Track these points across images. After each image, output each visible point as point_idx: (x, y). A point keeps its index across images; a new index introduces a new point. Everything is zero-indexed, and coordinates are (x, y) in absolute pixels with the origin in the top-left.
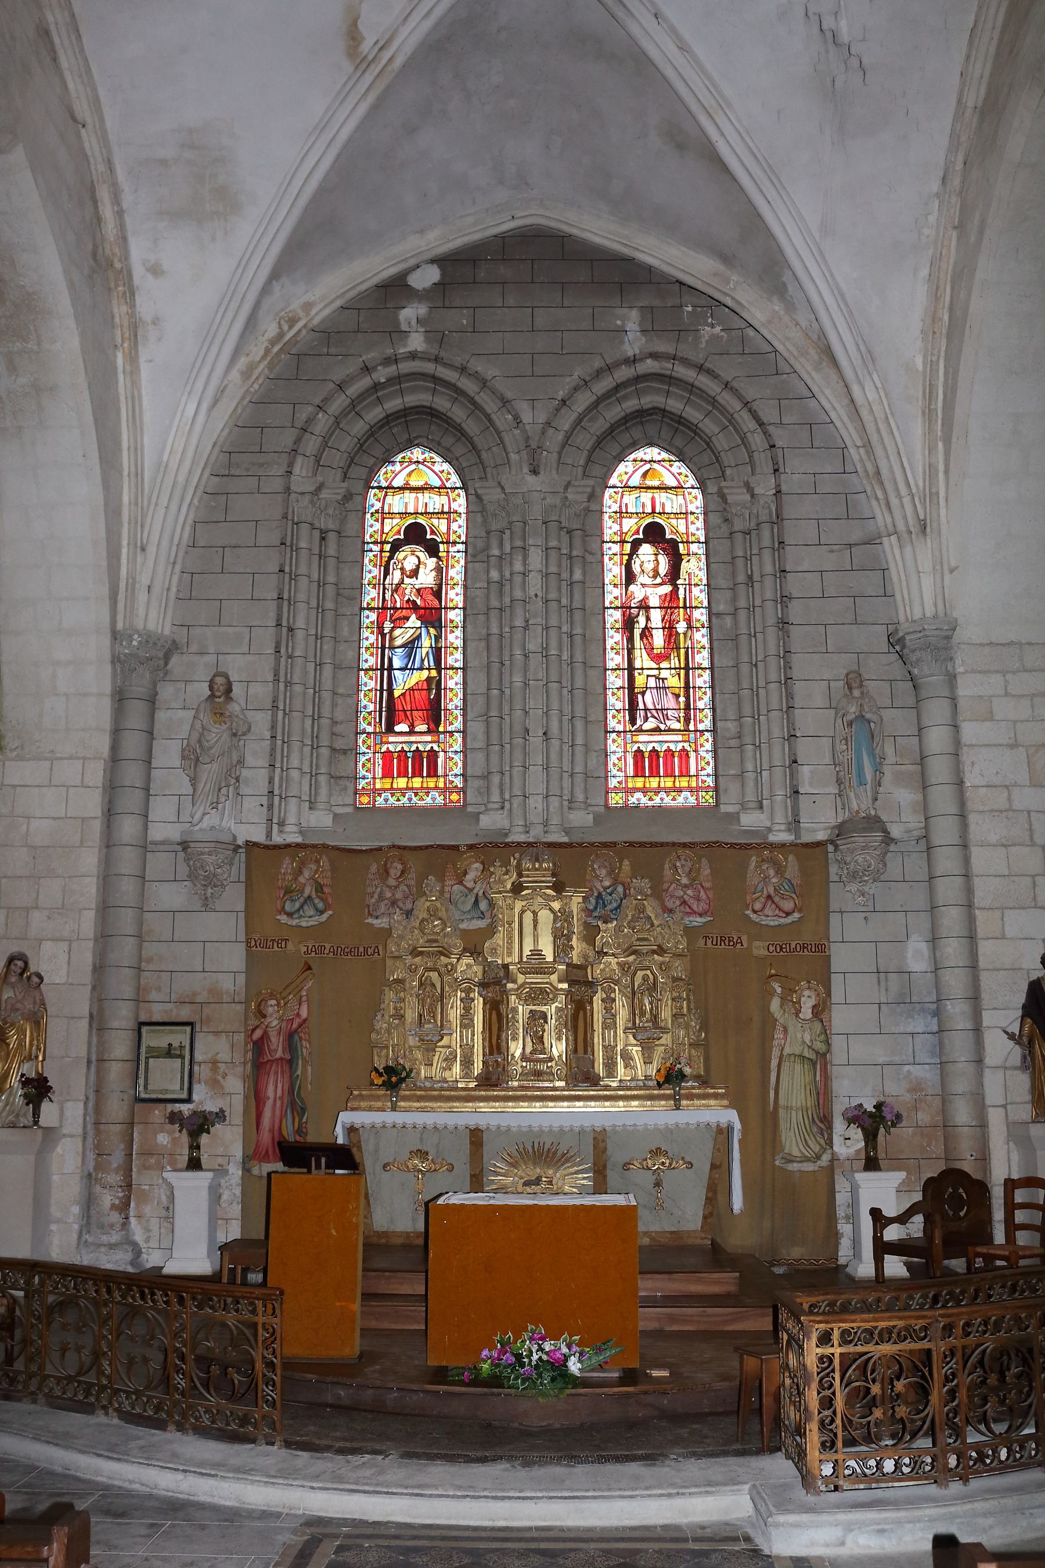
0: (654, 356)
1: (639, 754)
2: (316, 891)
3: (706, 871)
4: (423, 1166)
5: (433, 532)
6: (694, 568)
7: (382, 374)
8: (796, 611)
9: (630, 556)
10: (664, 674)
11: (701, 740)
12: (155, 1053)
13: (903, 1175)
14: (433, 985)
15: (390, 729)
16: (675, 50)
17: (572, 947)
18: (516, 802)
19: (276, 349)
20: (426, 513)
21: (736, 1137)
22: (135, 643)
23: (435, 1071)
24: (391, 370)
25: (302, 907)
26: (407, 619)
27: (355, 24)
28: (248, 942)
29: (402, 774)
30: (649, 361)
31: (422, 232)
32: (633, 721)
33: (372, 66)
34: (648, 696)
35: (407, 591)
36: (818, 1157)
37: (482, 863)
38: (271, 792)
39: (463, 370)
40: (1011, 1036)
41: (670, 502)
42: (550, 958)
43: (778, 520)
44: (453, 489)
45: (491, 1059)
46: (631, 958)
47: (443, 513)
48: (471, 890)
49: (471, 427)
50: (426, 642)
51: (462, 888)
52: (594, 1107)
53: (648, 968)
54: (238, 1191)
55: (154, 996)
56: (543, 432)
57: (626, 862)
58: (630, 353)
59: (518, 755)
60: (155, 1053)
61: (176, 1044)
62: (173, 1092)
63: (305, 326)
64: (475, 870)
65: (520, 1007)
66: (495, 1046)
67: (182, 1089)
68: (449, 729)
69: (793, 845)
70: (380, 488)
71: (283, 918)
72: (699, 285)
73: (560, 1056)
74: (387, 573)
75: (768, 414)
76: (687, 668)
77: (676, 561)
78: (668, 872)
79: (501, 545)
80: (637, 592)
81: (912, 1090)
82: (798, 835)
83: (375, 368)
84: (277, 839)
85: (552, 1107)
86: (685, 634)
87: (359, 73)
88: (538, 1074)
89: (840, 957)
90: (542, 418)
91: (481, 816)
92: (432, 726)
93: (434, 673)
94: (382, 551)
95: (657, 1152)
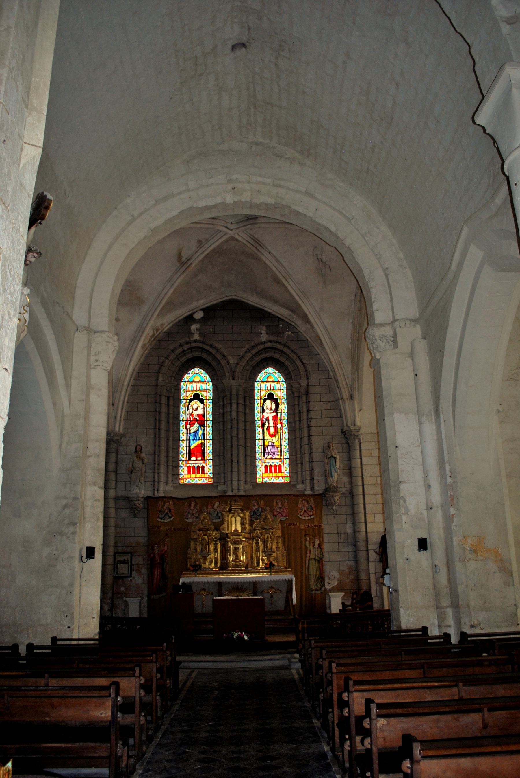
0: (270, 341)
1: (266, 466)
2: (169, 511)
3: (286, 503)
4: (205, 593)
5: (202, 396)
6: (283, 407)
7: (186, 347)
8: (313, 423)
9: (263, 403)
10: (274, 441)
11: (285, 462)
12: (120, 562)
13: (343, 593)
14: (206, 540)
15: (190, 460)
16: (275, 262)
17: (246, 528)
18: (229, 483)
19: (152, 339)
20: (200, 390)
21: (294, 583)
22: (112, 435)
23: (207, 565)
24: (189, 346)
25: (164, 516)
26: (194, 424)
27: (180, 253)
28: (148, 527)
29: (194, 473)
30: (269, 343)
31: (198, 301)
32: (264, 456)
33: (185, 265)
34: (269, 448)
35: (194, 415)
36: (321, 589)
37: (219, 502)
38: (154, 481)
39: (211, 346)
40: (376, 552)
42: (240, 531)
44: (208, 382)
45: (223, 561)
46: (264, 531)
47: (205, 390)
48: (216, 510)
49: (214, 363)
50: (201, 432)
51: (213, 509)
52: (253, 575)
53: (268, 534)
54: (146, 604)
55: (119, 544)
56: (236, 366)
57: (262, 501)
58: (263, 340)
59: (229, 468)
60: (120, 562)
61: (126, 559)
62: (126, 574)
63: (161, 332)
64: (217, 504)
65: (232, 546)
66: (224, 557)
67: (128, 573)
68: (208, 459)
69: (312, 495)
70: (185, 382)
71: (159, 520)
72: (284, 319)
73: (243, 560)
74: (188, 409)
75: (306, 361)
76: (281, 439)
77: (277, 405)
78: (275, 504)
79: (223, 402)
80: (266, 415)
81: (349, 569)
82: (314, 493)
83: (183, 345)
84: (156, 495)
85: (241, 576)
86: (280, 428)
87: (181, 266)
88: (237, 566)
89: (326, 528)
90: (236, 361)
91: (218, 487)
92: (203, 458)
93: (203, 441)
94: (186, 402)
95: (272, 588)
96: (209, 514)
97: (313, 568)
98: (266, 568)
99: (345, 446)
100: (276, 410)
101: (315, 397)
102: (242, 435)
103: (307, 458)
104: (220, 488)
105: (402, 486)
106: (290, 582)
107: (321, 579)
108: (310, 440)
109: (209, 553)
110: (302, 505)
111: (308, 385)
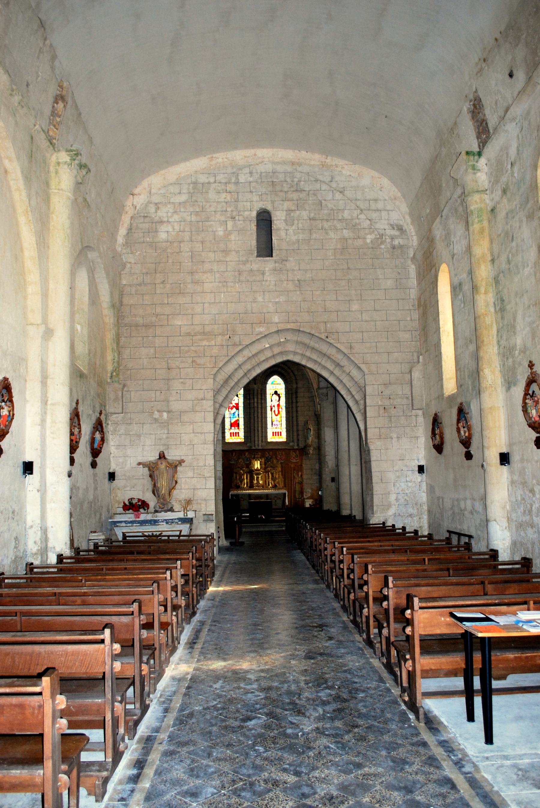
8: (299, 409)
43: (296, 393)
50: (236, 414)
52: (267, 491)
75: (296, 373)
77: (280, 397)
96: (243, 459)
97: (298, 487)
98: (273, 487)
99: (317, 422)
100: (279, 400)
101: (300, 394)
102: (260, 416)
103: (295, 428)
104: (248, 445)
105: (327, 457)
106: (285, 494)
107: (302, 493)
108: (297, 419)
109: (244, 479)
110: (293, 454)
111: (297, 387)
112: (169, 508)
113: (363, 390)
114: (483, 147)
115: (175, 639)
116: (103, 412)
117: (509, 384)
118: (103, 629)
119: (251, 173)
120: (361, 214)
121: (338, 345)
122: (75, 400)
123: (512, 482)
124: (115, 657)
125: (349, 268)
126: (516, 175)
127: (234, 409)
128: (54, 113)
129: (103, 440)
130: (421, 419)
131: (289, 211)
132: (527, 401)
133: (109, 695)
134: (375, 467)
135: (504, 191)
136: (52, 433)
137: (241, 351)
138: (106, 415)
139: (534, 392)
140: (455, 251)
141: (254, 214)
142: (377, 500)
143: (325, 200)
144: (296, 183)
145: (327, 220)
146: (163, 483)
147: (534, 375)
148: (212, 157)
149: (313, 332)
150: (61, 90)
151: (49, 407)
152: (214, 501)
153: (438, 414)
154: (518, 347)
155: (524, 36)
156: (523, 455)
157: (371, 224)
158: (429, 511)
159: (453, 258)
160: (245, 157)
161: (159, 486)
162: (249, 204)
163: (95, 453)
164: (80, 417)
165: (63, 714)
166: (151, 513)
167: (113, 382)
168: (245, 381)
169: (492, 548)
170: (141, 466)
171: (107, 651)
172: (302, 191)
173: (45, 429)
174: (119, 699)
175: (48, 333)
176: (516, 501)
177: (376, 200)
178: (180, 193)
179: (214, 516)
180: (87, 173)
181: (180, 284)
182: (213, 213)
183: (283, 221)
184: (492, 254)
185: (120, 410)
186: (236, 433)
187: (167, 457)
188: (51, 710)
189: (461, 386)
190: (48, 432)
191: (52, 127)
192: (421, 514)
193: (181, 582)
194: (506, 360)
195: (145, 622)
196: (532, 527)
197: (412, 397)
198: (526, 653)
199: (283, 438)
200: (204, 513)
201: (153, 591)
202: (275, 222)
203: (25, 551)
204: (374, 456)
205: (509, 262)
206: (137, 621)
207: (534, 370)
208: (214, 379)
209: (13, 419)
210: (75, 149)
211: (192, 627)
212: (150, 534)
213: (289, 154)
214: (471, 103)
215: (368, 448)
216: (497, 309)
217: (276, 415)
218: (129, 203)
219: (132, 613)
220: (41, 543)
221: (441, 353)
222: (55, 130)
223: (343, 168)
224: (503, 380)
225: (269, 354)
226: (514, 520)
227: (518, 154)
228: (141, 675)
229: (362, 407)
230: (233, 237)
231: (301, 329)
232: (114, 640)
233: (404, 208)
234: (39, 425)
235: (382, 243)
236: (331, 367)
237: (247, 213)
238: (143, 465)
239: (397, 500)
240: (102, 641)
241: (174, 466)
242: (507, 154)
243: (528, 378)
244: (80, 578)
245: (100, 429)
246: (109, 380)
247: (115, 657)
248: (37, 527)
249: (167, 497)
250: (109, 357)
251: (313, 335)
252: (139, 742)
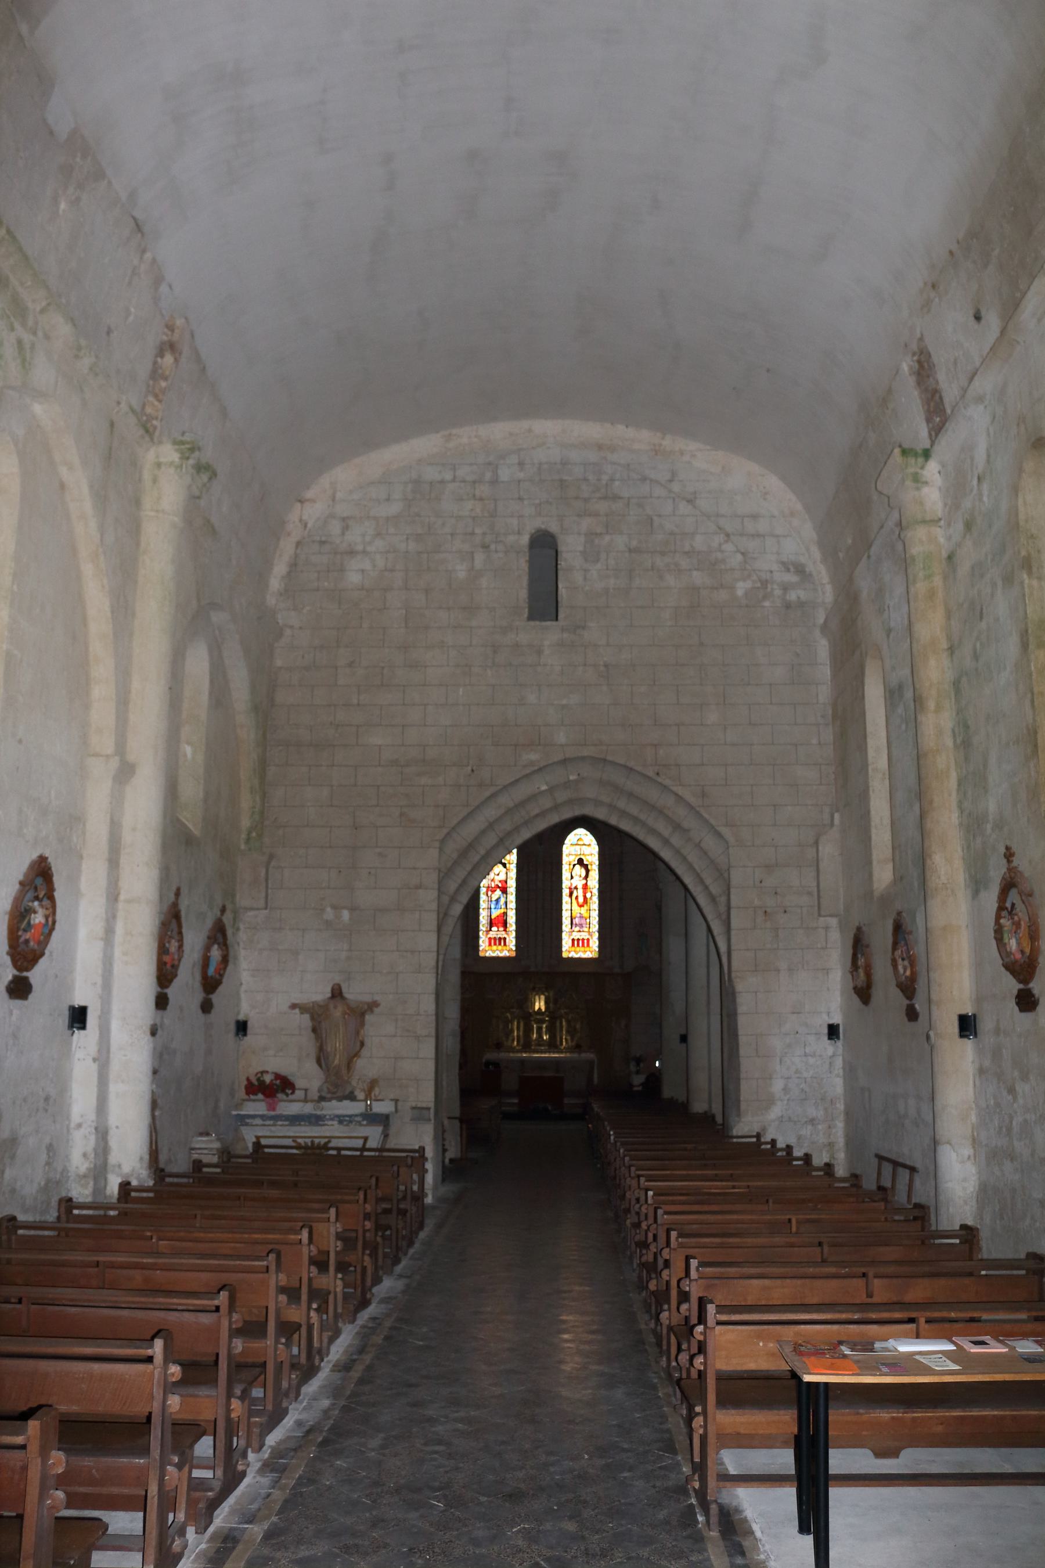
15: (491, 930)
34: (577, 919)
41: (586, 850)
50: (503, 900)
77: (588, 871)
109: (512, 1031)
112: (347, 1092)
113: (726, 875)
114: (937, 435)
115: (314, 1352)
116: (229, 906)
117: (977, 885)
118: (153, 1338)
119: (521, 464)
120: (726, 542)
121: (680, 791)
122: (174, 889)
123: (981, 1071)
124: (170, 1388)
125: (701, 644)
126: (985, 499)
127: (498, 892)
128: (156, 373)
129: (225, 960)
130: (835, 935)
131: (591, 535)
132: (1002, 921)
133: (156, 1452)
134: (744, 1023)
135: (968, 526)
136: (125, 954)
137: (493, 796)
138: (235, 912)
139: (1013, 905)
140: (892, 624)
141: (525, 539)
142: (746, 1090)
143: (660, 516)
144: (604, 482)
145: (663, 554)
146: (337, 1044)
147: (1013, 875)
148: (450, 434)
149: (631, 764)
150: (169, 333)
151: (121, 905)
152: (432, 1083)
153: (864, 929)
154: (991, 818)
155: (996, 252)
156: (998, 1021)
157: (745, 562)
158: (847, 1113)
159: (888, 636)
160: (511, 434)
161: (329, 1049)
162: (515, 522)
163: (210, 984)
164: (183, 920)
165: (61, 1481)
166: (312, 1101)
167: (250, 849)
168: (526, 834)
169: (918, 1201)
170: (297, 1011)
171: (156, 1376)
172: (616, 498)
173: (112, 947)
174: (176, 1459)
175: (126, 772)
176: (988, 1106)
177: (755, 517)
178: (388, 500)
179: (432, 1111)
180: (210, 479)
181: (383, 668)
182: (449, 537)
183: (578, 554)
184: (949, 638)
185: (262, 903)
186: (500, 939)
187: (346, 995)
188: (39, 1475)
189: (902, 878)
190: (117, 952)
191: (151, 398)
192: (833, 1120)
193: (334, 1246)
194: (972, 838)
195: (240, 1325)
196: (1012, 1160)
197: (819, 891)
198: (914, 1412)
199: (591, 951)
200: (414, 1104)
201: (268, 1267)
202: (564, 555)
203: (65, 1170)
204: (744, 1003)
205: (976, 657)
206: (225, 1323)
207: (1014, 864)
208: (441, 849)
209: (52, 929)
210: (189, 439)
211: (356, 1331)
212: (309, 1141)
213: (593, 431)
214: (915, 358)
215: (733, 988)
216: (958, 741)
217: (581, 906)
218: (293, 516)
219: (217, 1309)
220: (95, 1158)
221: (869, 812)
222: (156, 403)
223: (693, 456)
224: (967, 876)
225: (546, 803)
226: (984, 1144)
227: (988, 461)
228: (228, 1420)
229: (722, 908)
230: (484, 582)
231: (609, 758)
232: (167, 1359)
233: (809, 531)
234: (102, 939)
235: (765, 597)
236: (665, 830)
237: (511, 538)
238: (300, 1008)
239: (786, 1090)
240: (150, 1359)
241: (361, 1012)
242: (972, 459)
243: (1003, 878)
244: (149, 1234)
245: (221, 940)
246: (243, 847)
247: (170, 1388)
248: (90, 1126)
249: (344, 1071)
250: (246, 801)
251: (631, 769)
252: (212, 1539)
